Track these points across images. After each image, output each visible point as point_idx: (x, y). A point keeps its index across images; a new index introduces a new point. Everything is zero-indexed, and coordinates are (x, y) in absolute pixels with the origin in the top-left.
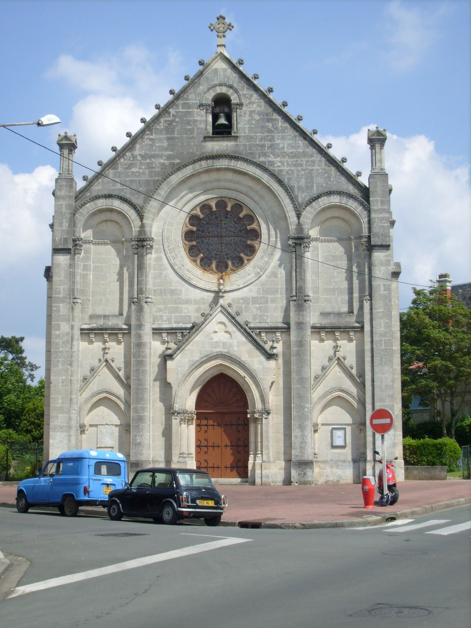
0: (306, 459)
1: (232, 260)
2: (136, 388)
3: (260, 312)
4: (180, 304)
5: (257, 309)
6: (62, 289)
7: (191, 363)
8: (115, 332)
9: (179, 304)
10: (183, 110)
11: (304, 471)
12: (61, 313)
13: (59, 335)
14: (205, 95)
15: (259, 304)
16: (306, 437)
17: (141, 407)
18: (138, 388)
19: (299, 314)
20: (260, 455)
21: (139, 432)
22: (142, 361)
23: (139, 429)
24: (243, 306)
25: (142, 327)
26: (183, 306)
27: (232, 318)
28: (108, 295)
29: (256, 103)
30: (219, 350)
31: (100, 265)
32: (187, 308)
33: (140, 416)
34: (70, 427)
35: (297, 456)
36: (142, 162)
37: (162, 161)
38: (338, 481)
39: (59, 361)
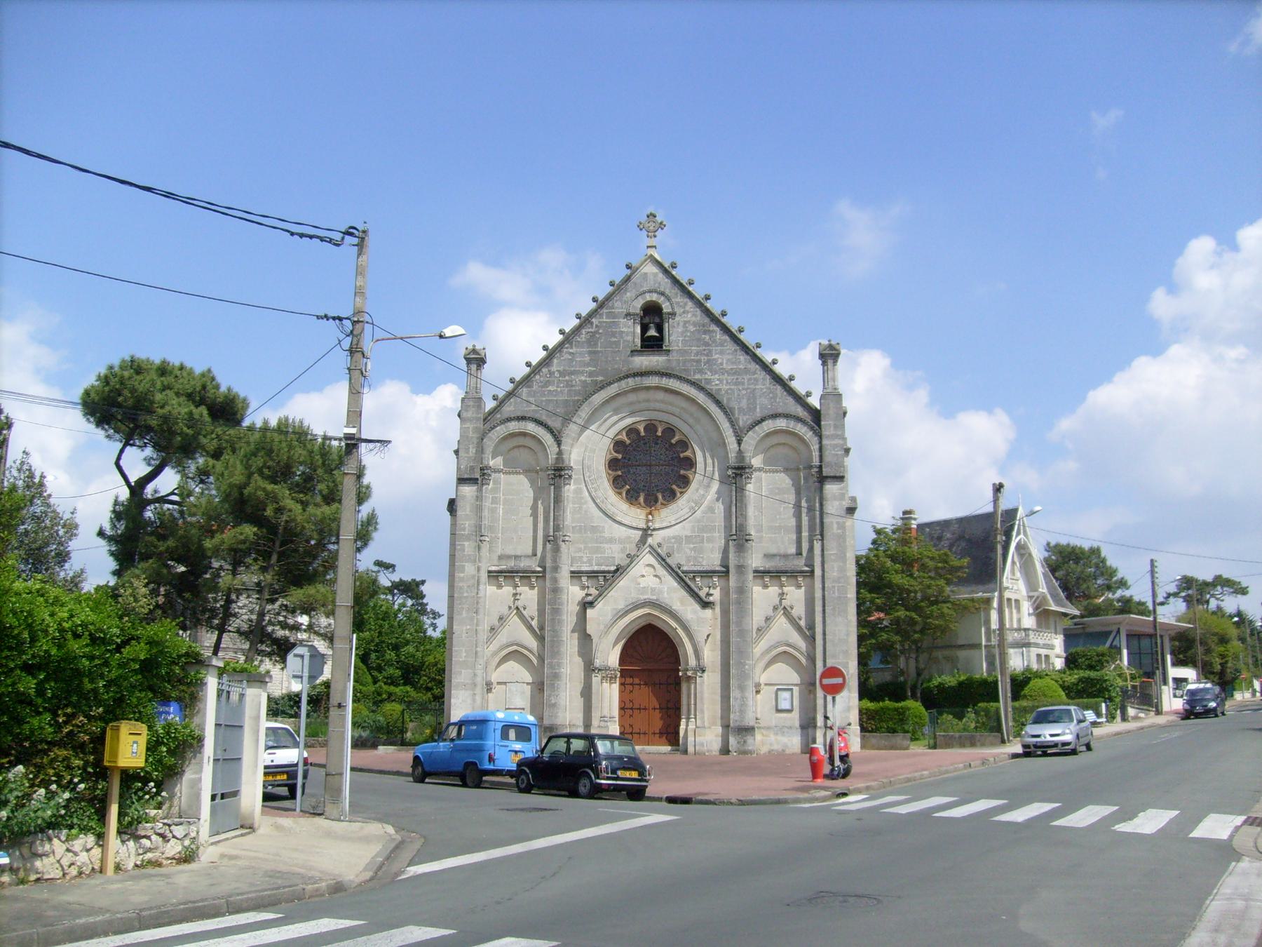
5: (691, 550)
27: (662, 560)
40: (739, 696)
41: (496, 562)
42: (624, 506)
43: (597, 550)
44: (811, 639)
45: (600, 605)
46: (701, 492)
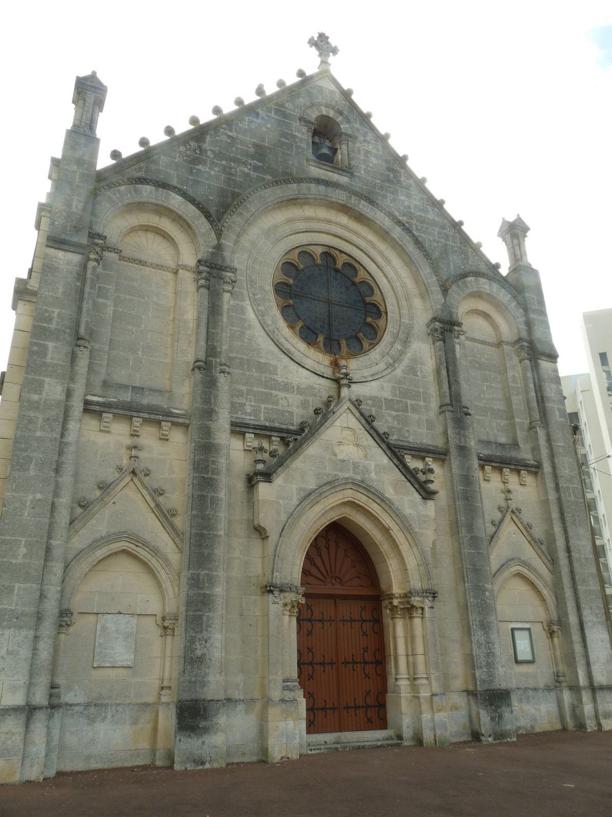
0: (498, 687)
1: (347, 339)
2: (197, 534)
3: (399, 423)
4: (275, 389)
5: (394, 418)
6: (55, 314)
7: (303, 494)
8: (157, 417)
9: (271, 389)
10: (276, 117)
11: (499, 710)
12: (48, 360)
13: (38, 402)
14: (307, 111)
15: (397, 410)
16: (493, 644)
17: (208, 575)
18: (202, 536)
19: (459, 434)
20: (425, 682)
21: (201, 631)
22: (211, 479)
23: (201, 625)
24: (373, 409)
25: (214, 415)
26: (281, 395)
27: (368, 421)
28: (140, 353)
29: (372, 143)
30: (348, 475)
31: (128, 297)
32: (286, 398)
33: (205, 595)
34: (39, 617)
35: (484, 682)
36: (215, 161)
37: (246, 170)
38: (532, 727)
39: (30, 459)
40: (483, 639)
41: (98, 390)
42: (302, 346)
43: (267, 398)
44: (553, 561)
45: (279, 480)
46: (398, 346)
